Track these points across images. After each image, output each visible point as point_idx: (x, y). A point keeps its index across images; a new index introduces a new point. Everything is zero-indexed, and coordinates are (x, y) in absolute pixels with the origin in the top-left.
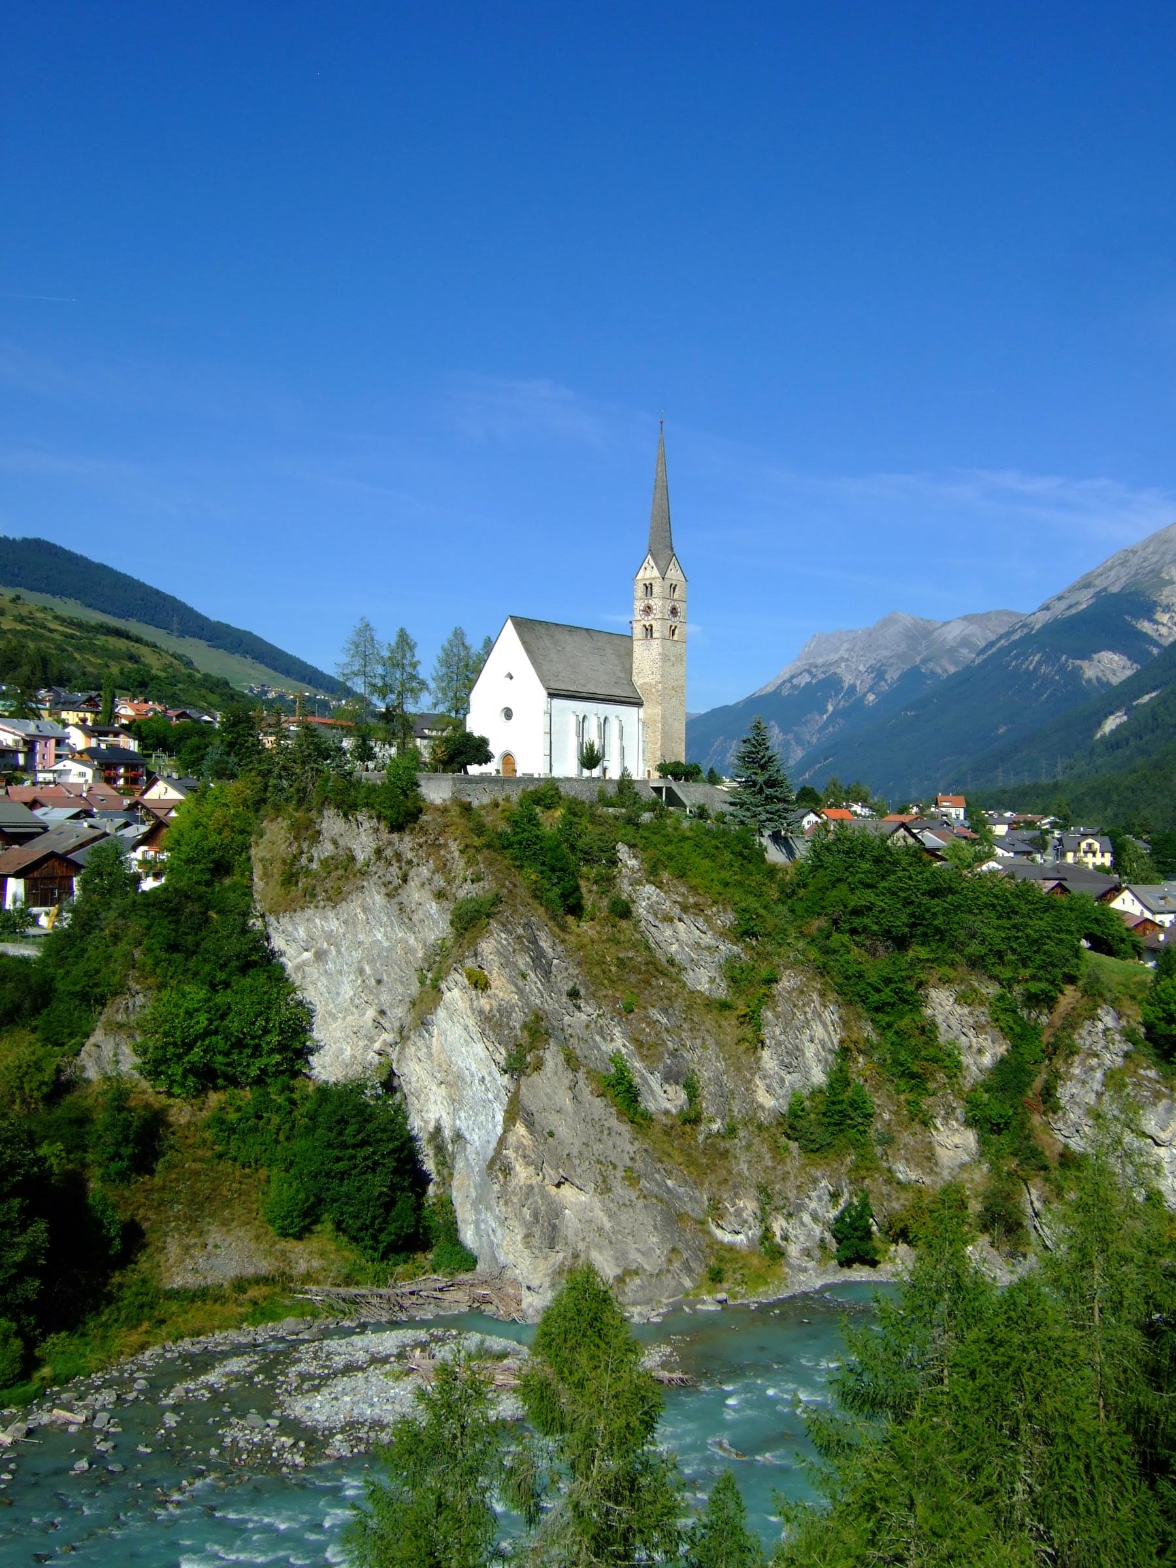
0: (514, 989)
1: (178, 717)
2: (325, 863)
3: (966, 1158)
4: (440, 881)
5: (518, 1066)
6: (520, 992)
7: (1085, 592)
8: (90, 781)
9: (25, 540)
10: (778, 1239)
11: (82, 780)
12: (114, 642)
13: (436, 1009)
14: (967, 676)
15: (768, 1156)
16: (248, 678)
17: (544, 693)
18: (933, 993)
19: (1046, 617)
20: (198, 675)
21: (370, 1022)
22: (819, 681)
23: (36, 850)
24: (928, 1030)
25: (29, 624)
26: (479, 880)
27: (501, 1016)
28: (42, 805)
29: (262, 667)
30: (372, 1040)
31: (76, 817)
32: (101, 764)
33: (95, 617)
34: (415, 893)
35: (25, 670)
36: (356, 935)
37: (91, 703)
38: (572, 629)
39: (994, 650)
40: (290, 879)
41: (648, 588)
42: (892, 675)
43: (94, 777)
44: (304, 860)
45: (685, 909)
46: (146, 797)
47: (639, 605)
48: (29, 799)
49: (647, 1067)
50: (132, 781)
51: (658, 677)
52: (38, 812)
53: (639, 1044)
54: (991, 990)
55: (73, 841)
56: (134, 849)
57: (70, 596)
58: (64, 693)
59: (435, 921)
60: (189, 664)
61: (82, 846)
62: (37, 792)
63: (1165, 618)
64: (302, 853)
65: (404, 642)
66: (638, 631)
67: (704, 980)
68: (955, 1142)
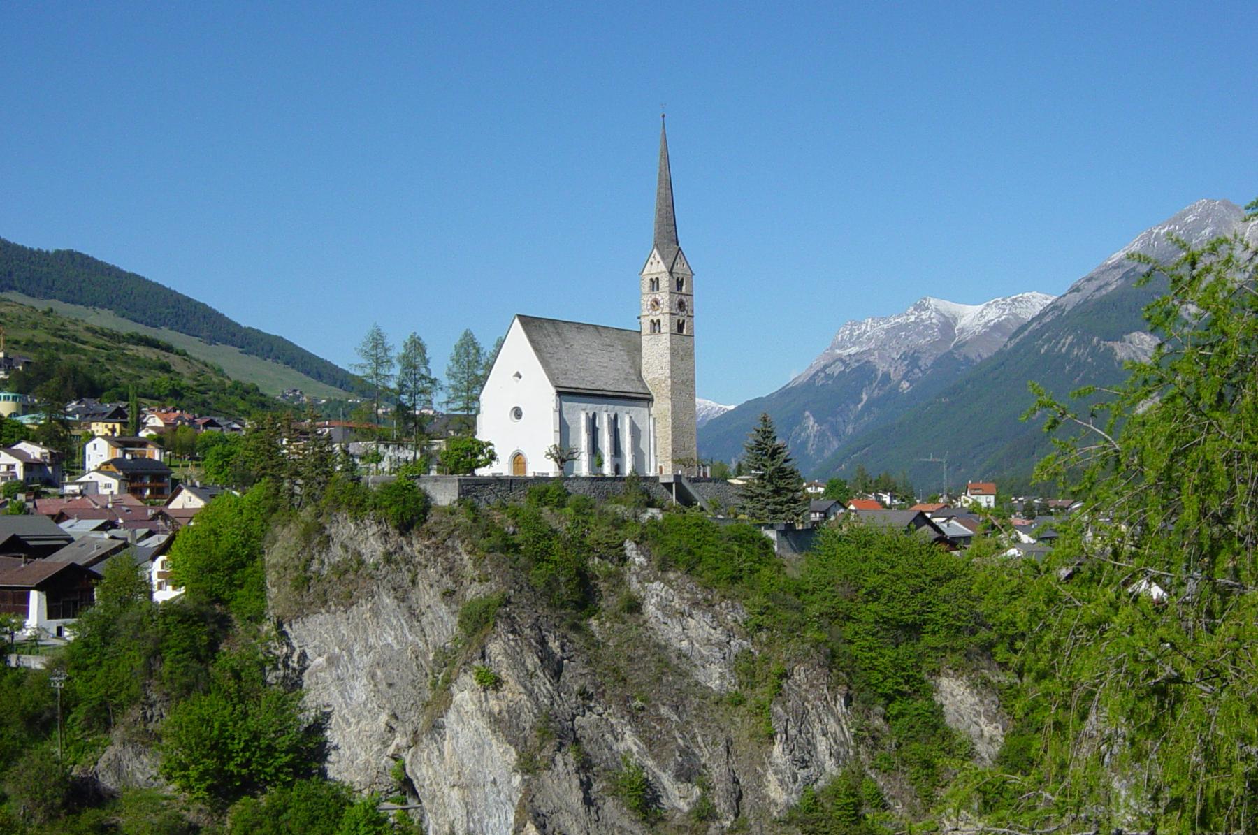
0: (522, 690)
1: (206, 425)
2: (335, 567)
4: (448, 582)
5: (528, 765)
6: (530, 693)
7: (1115, 272)
8: (116, 492)
9: (58, 252)
11: (107, 492)
12: (142, 351)
13: (446, 711)
14: (1002, 361)
16: (276, 382)
17: (553, 391)
18: (944, 681)
19: (1077, 298)
20: (228, 383)
21: (383, 726)
22: (853, 371)
23: (61, 559)
25: (62, 337)
26: (487, 580)
27: (511, 717)
28: (68, 518)
29: (294, 372)
30: (385, 744)
31: (101, 528)
32: (127, 475)
33: (127, 327)
34: (427, 596)
35: (54, 383)
37: (118, 415)
38: (580, 326)
39: (1026, 333)
40: (303, 583)
41: (655, 283)
42: (926, 361)
43: (120, 487)
44: (315, 565)
45: (695, 604)
46: (171, 506)
47: (647, 300)
48: (56, 511)
49: (658, 765)
50: (158, 492)
51: (668, 373)
52: (64, 526)
53: (650, 743)
55: (95, 553)
56: (153, 559)
57: (102, 307)
58: (94, 404)
59: (443, 624)
60: (220, 372)
61: (102, 557)
62: (63, 504)
64: (313, 558)
65: (416, 347)
66: (646, 328)
67: (714, 677)
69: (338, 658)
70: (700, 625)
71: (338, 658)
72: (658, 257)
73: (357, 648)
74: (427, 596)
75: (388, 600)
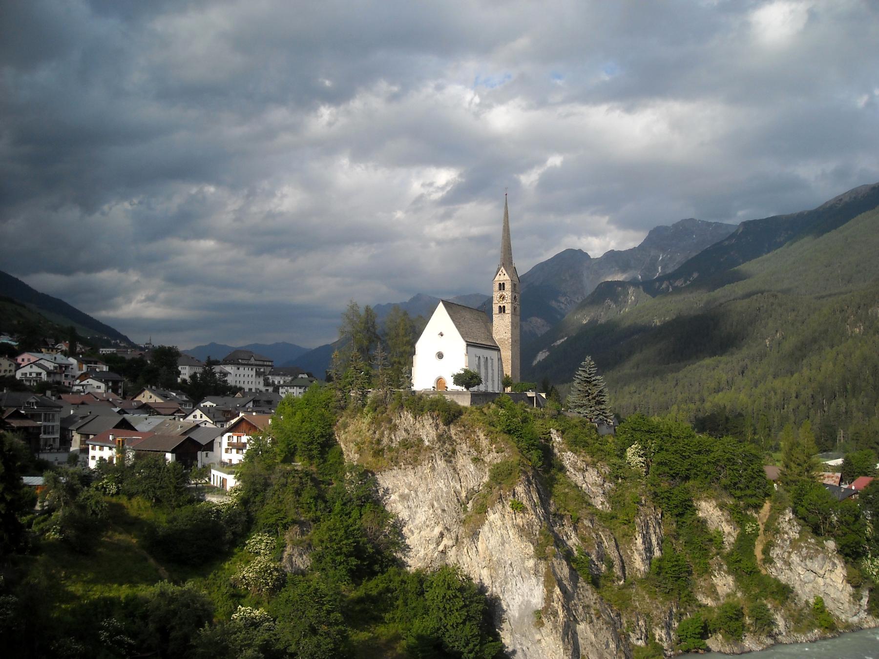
3: (729, 591)
10: (657, 641)
15: (647, 596)
17: (464, 344)
24: (703, 522)
30: (438, 544)
34: (464, 462)
36: (427, 485)
51: (509, 335)
54: (731, 502)
63: (563, 300)
67: (599, 502)
68: (724, 583)
69: (408, 495)
70: (592, 476)
71: (408, 495)
72: (504, 272)
73: (420, 490)
74: (464, 462)
75: (441, 464)
